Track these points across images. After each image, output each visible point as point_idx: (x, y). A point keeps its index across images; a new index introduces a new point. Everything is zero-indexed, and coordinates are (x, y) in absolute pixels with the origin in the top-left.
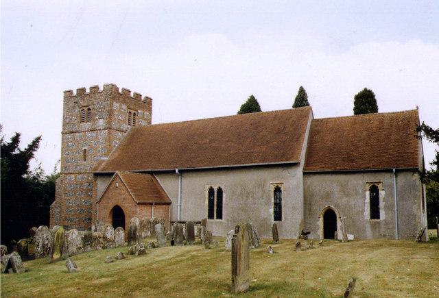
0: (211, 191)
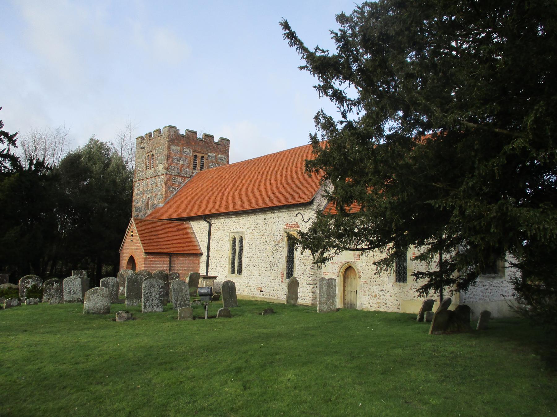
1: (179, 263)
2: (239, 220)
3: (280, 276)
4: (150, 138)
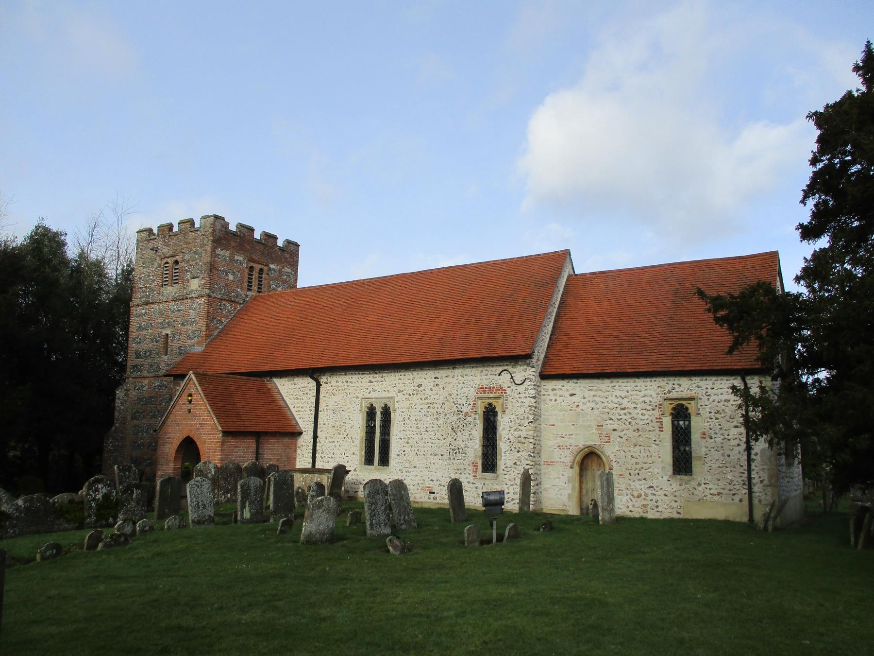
0: (371, 413)
1: (270, 449)
2: (380, 379)
3: (471, 468)
4: (171, 234)
